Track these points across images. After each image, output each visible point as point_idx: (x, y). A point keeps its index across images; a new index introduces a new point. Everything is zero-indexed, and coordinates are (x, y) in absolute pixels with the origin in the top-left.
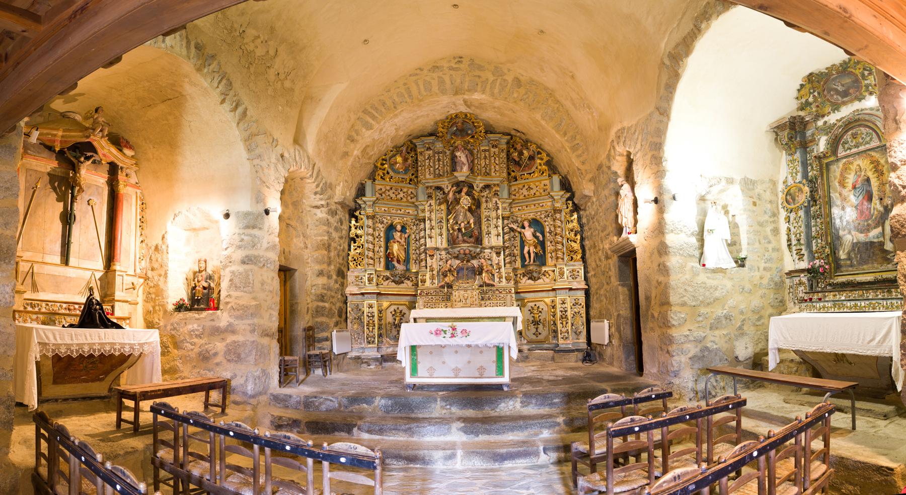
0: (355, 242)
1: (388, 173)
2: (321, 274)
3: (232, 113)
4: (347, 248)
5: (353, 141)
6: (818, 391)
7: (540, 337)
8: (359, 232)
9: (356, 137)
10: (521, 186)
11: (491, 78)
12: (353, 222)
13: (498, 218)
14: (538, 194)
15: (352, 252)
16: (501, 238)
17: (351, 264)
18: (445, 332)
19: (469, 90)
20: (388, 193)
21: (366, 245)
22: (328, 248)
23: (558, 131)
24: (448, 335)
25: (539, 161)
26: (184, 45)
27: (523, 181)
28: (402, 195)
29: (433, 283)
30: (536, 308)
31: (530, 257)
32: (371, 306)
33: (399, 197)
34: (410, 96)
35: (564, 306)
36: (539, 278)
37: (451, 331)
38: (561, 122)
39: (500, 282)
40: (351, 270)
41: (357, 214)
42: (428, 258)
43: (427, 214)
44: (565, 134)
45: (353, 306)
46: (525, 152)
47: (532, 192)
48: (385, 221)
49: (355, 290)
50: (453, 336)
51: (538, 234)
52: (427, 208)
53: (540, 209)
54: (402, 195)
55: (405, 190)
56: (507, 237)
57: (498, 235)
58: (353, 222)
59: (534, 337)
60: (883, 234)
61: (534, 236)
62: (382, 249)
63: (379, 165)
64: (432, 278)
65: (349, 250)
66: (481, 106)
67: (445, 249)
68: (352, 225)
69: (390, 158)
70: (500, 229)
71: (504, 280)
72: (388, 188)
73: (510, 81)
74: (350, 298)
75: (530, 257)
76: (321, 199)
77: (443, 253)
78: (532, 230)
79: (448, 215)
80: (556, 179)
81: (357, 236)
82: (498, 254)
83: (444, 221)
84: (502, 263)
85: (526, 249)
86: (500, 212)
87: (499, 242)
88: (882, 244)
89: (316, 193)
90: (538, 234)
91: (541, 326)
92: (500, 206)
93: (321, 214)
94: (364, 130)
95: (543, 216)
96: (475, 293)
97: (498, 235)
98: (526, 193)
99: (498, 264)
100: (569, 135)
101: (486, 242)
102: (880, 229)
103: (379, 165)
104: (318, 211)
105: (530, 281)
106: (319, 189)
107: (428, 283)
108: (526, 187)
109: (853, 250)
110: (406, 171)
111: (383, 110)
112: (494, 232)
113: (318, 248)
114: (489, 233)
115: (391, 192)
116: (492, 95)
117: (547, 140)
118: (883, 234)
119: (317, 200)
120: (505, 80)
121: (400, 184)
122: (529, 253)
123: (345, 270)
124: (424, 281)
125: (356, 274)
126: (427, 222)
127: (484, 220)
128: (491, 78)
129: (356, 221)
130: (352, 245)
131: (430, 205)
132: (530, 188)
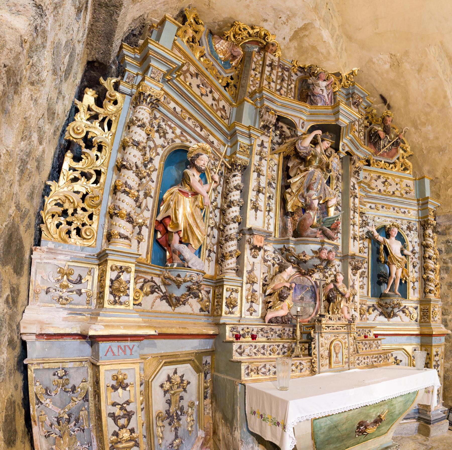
0: (77, 159)
6: (230, 416)
8: (98, 133)
10: (374, 175)
12: (90, 97)
14: (397, 193)
15: (61, 188)
17: (51, 223)
20: (189, 80)
25: (401, 151)
29: (251, 311)
40: (46, 244)
41: (108, 83)
42: (247, 253)
45: (49, 379)
48: (170, 136)
49: (59, 320)
53: (401, 216)
55: (217, 96)
58: (90, 97)
68: (82, 106)
74: (35, 350)
105: (382, 319)
110: (226, 64)
123: (28, 240)
129: (99, 102)
130: (68, 161)
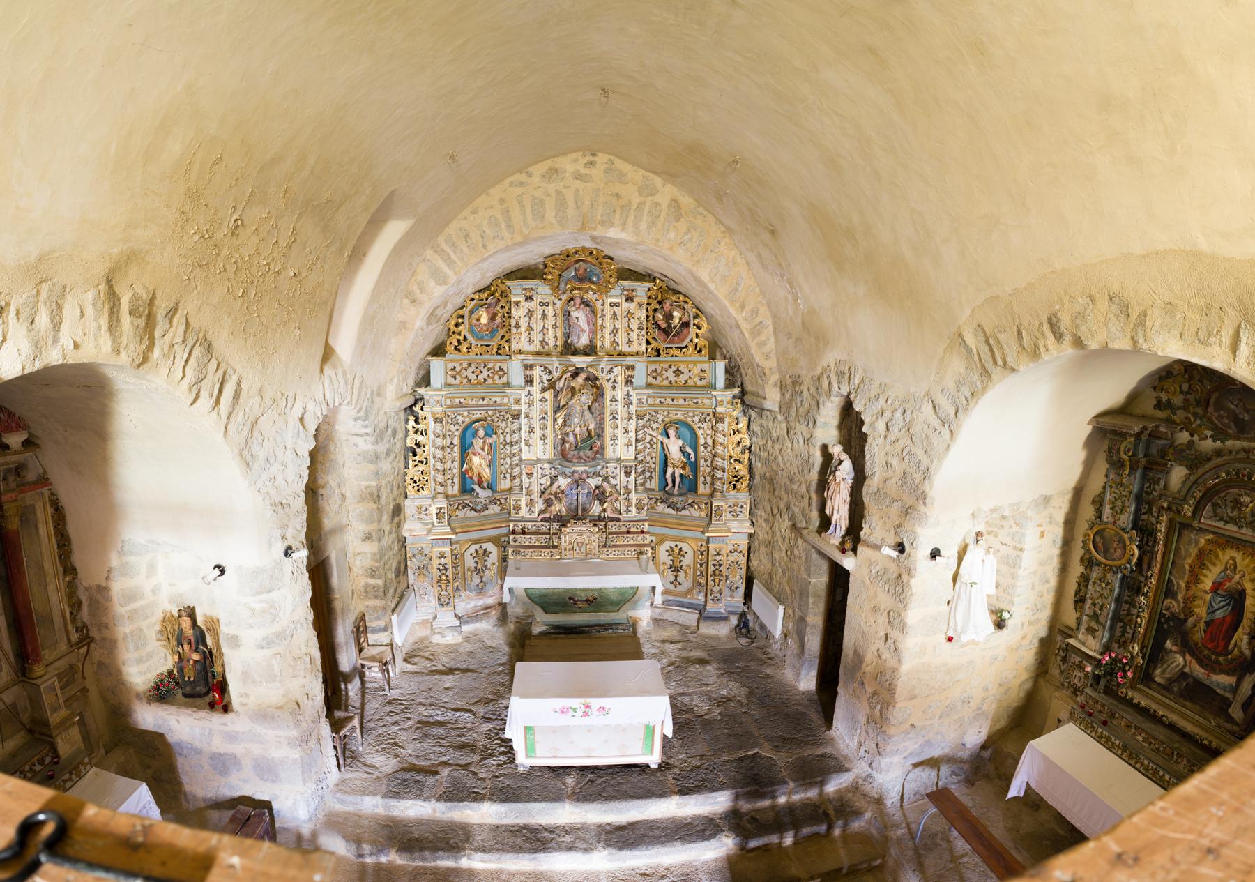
1: (465, 339)
2: (368, 537)
3: (214, 413)
4: (402, 465)
5: (413, 301)
7: (679, 588)
9: (418, 295)
11: (636, 200)
13: (630, 418)
16: (632, 449)
18: (575, 710)
19: (602, 223)
20: (464, 373)
21: (432, 461)
22: (376, 498)
23: (732, 302)
24: (580, 713)
26: (105, 326)
27: (669, 359)
28: (485, 374)
30: (677, 550)
31: (674, 482)
32: (442, 556)
33: (481, 377)
34: (509, 226)
35: (718, 558)
36: (683, 509)
37: (583, 709)
38: (738, 284)
39: (628, 511)
43: (523, 408)
44: (743, 306)
46: (676, 314)
47: (683, 378)
48: (460, 419)
50: (586, 714)
51: (688, 450)
52: (524, 400)
54: (485, 374)
55: (490, 365)
56: (640, 446)
57: (629, 444)
58: (412, 423)
59: (672, 587)
60: (1235, 689)
61: (682, 450)
62: (456, 464)
63: (452, 327)
64: (531, 503)
65: (406, 466)
66: (617, 243)
67: (550, 462)
69: (471, 312)
70: (632, 435)
71: (633, 509)
72: (465, 365)
73: (664, 206)
75: (674, 482)
76: (366, 427)
77: (547, 466)
78: (680, 442)
79: (555, 412)
80: (721, 366)
81: (418, 445)
82: (628, 474)
83: (550, 418)
84: (632, 486)
85: (670, 471)
86: (633, 408)
87: (630, 454)
88: (1227, 703)
89: (356, 419)
90: (688, 450)
91: (681, 575)
92: (634, 399)
93: (365, 445)
94: (432, 284)
95: (696, 419)
96: (593, 538)
97: (629, 444)
98: (672, 378)
99: (626, 487)
100: (748, 308)
101: (610, 452)
102: (1231, 680)
103: (452, 327)
104: (360, 441)
106: (362, 413)
107: (524, 512)
108: (674, 369)
109: (1177, 680)
111: (465, 249)
112: (622, 439)
113: (362, 498)
114: (614, 438)
115: (470, 370)
116: (637, 231)
117: (711, 304)
118: (1235, 689)
119: (358, 427)
120: (657, 204)
121: (485, 357)
122: (673, 475)
124: (517, 508)
125: (418, 503)
126: (524, 421)
127: (608, 418)
128: (636, 200)
129: (416, 421)
131: (529, 394)
132: (678, 372)
